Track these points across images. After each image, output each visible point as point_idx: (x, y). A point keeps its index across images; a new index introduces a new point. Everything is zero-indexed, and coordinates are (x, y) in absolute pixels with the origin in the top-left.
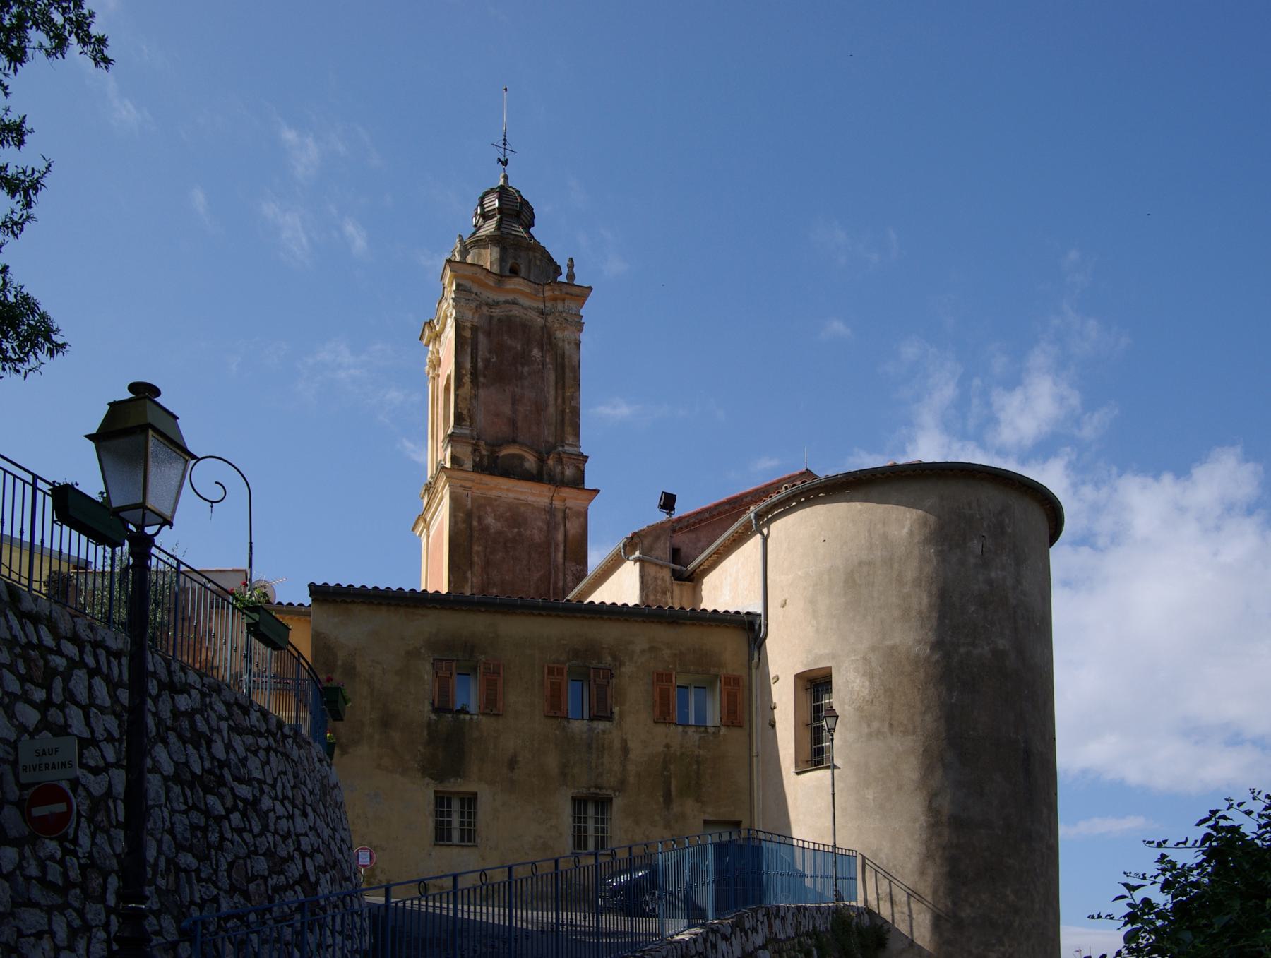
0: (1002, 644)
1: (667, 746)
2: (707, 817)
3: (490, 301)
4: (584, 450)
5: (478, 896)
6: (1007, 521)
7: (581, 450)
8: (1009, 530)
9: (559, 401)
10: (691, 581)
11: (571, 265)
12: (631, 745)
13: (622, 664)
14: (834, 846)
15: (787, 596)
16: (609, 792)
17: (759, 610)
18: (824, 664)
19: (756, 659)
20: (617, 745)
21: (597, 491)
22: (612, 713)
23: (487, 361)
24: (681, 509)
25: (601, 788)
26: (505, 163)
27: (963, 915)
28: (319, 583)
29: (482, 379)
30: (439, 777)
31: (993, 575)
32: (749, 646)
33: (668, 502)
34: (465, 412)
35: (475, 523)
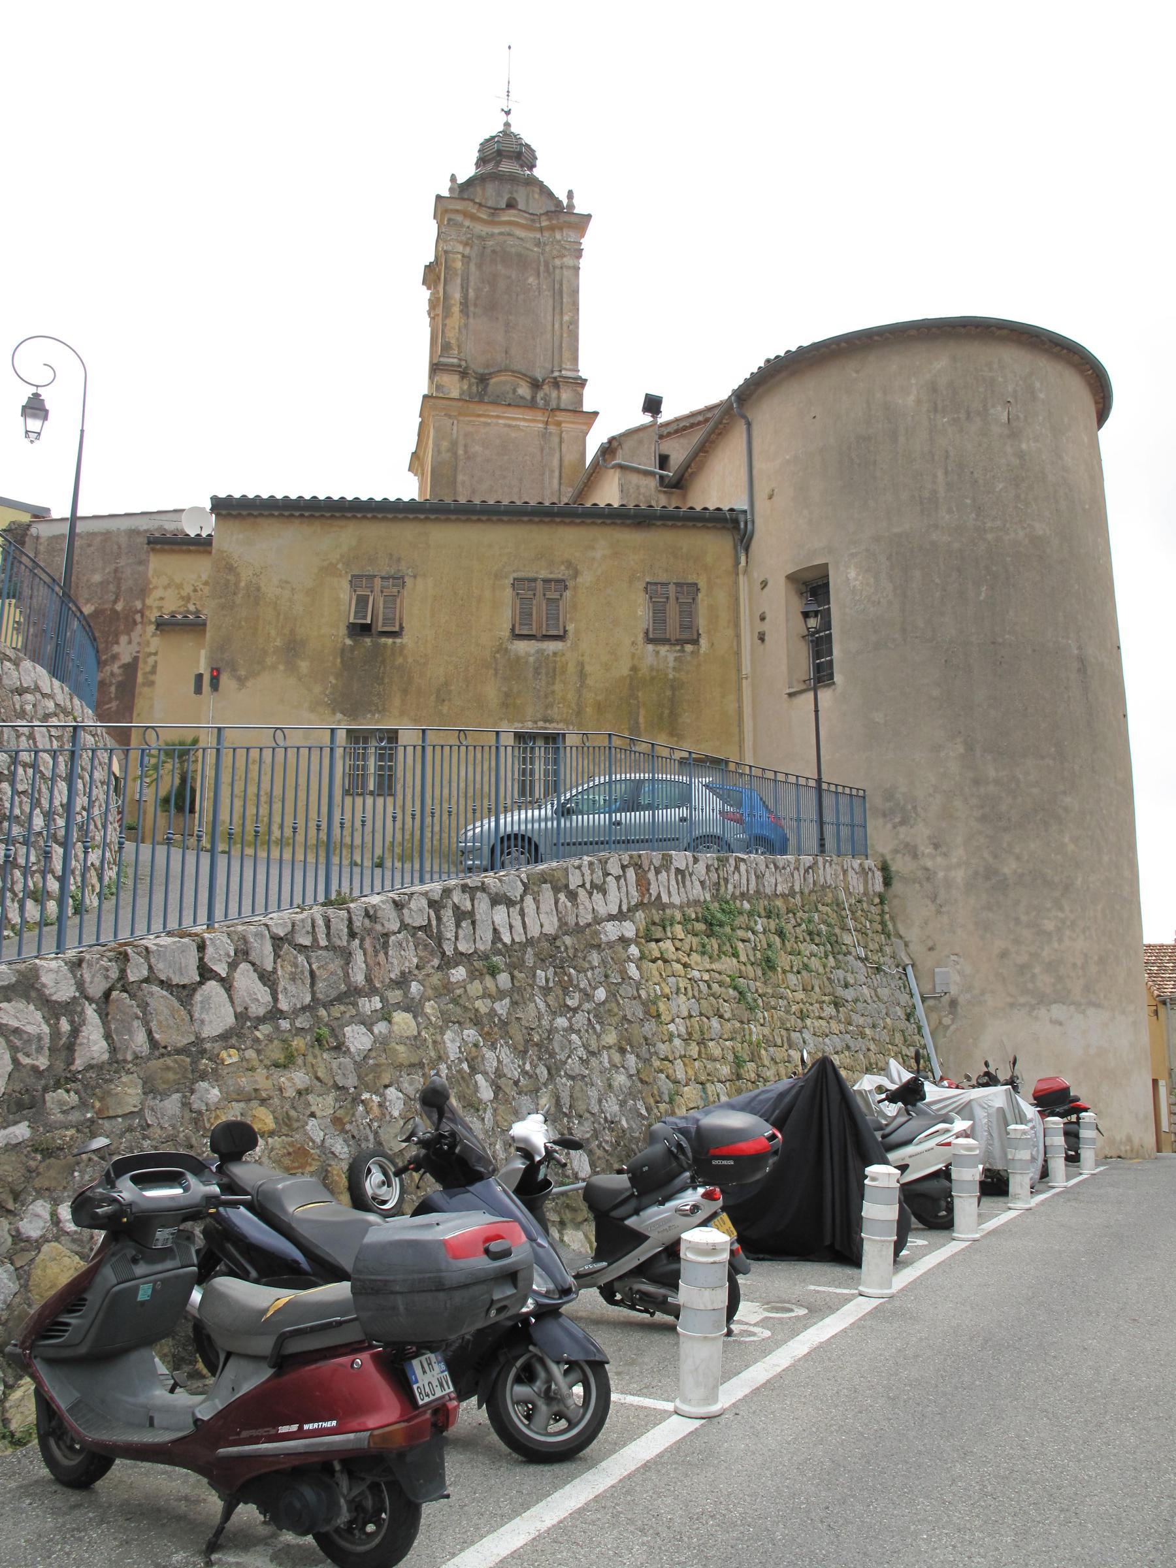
0: (1040, 528)
1: (634, 669)
3: (483, 233)
4: (583, 374)
6: (1038, 385)
8: (1042, 396)
12: (588, 668)
13: (576, 574)
14: (819, 781)
17: (742, 504)
19: (743, 562)
20: (572, 668)
21: (596, 414)
22: (565, 631)
23: (478, 290)
24: (668, 413)
25: (551, 721)
26: (508, 113)
27: (1006, 870)
28: (222, 495)
29: (472, 309)
30: (352, 712)
31: (1024, 446)
32: (735, 547)
33: (652, 405)
34: (453, 341)
35: (461, 452)
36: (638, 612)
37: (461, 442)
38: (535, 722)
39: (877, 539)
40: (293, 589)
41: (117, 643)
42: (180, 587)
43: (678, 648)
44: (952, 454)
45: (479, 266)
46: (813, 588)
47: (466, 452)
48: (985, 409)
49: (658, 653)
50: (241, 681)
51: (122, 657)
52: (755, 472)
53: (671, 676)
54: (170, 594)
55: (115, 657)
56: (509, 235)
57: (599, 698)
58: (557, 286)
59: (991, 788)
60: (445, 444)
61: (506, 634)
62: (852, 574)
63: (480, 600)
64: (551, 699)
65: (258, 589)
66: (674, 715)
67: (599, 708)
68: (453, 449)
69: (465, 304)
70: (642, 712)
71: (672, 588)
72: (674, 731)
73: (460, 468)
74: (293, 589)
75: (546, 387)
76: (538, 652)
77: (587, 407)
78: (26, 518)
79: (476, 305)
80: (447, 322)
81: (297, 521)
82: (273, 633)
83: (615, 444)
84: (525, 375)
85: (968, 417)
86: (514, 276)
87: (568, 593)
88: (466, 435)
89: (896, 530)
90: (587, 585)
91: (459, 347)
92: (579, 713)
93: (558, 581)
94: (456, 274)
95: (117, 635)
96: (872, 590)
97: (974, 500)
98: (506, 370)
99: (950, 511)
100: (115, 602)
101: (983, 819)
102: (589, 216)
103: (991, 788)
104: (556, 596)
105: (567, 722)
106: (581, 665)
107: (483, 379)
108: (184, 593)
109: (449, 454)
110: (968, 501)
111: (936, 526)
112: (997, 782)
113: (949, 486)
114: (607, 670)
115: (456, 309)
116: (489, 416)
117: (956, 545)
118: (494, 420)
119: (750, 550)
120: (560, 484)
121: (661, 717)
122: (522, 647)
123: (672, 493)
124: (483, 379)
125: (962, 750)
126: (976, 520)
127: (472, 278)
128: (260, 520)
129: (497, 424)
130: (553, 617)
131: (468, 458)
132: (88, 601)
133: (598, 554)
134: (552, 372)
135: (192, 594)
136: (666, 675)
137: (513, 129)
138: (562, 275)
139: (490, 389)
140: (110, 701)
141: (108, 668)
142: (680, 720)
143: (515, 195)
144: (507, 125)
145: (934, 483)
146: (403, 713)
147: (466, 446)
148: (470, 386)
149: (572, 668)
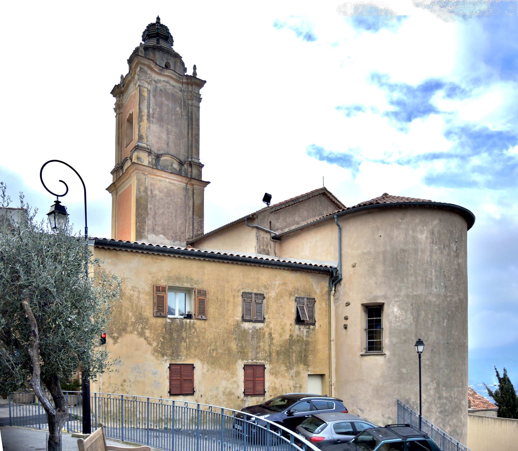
1: (291, 336)
2: (309, 373)
3: (156, 79)
4: (202, 161)
5: (183, 421)
7: (200, 161)
9: (190, 135)
10: (279, 240)
11: (195, 67)
15: (356, 261)
16: (263, 361)
18: (380, 301)
20: (267, 335)
21: (209, 183)
22: (264, 318)
24: (273, 202)
29: (151, 119)
32: (329, 283)
33: (267, 198)
34: (144, 135)
35: (149, 193)
36: (291, 309)
37: (149, 188)
38: (252, 360)
39: (408, 296)
40: (139, 292)
43: (308, 327)
44: (438, 263)
45: (154, 96)
46: (374, 312)
47: (152, 193)
48: (450, 245)
49: (300, 329)
50: (115, 340)
52: (343, 252)
56: (167, 82)
57: (277, 349)
58: (190, 115)
59: (444, 401)
60: (142, 189)
61: (239, 319)
62: (396, 309)
63: (228, 302)
64: (258, 350)
66: (306, 356)
67: (278, 353)
69: (148, 116)
70: (294, 355)
71: (305, 299)
72: (306, 363)
73: (149, 201)
74: (139, 292)
75: (185, 165)
76: (253, 328)
77: (204, 179)
79: (153, 117)
80: (141, 124)
81: (139, 255)
82: (130, 314)
83: (255, 216)
84: (177, 158)
85: (444, 247)
86: (170, 105)
87: (265, 301)
88: (151, 185)
89: (415, 293)
90: (273, 297)
92: (270, 356)
93: (261, 295)
96: (404, 318)
97: (444, 283)
98: (169, 154)
99: (436, 288)
101: (441, 412)
102: (205, 82)
103: (444, 401)
104: (260, 301)
105: (264, 359)
106: (270, 334)
107: (158, 157)
110: (442, 284)
111: (431, 294)
112: (446, 398)
113: (436, 276)
114: (281, 336)
115: (145, 118)
116: (162, 177)
117: (437, 303)
118: (164, 179)
120: (193, 214)
121: (301, 357)
122: (247, 325)
123: (276, 242)
124: (158, 157)
125: (435, 386)
126: (444, 292)
127: (151, 102)
128: (120, 253)
129: (165, 181)
130: (260, 311)
133: (277, 283)
134: (188, 158)
136: (303, 339)
137: (162, 22)
138: (192, 109)
139: (161, 162)
142: (308, 359)
143: (169, 61)
145: (431, 275)
146: (195, 356)
147: (151, 190)
148: (152, 159)
149: (267, 335)
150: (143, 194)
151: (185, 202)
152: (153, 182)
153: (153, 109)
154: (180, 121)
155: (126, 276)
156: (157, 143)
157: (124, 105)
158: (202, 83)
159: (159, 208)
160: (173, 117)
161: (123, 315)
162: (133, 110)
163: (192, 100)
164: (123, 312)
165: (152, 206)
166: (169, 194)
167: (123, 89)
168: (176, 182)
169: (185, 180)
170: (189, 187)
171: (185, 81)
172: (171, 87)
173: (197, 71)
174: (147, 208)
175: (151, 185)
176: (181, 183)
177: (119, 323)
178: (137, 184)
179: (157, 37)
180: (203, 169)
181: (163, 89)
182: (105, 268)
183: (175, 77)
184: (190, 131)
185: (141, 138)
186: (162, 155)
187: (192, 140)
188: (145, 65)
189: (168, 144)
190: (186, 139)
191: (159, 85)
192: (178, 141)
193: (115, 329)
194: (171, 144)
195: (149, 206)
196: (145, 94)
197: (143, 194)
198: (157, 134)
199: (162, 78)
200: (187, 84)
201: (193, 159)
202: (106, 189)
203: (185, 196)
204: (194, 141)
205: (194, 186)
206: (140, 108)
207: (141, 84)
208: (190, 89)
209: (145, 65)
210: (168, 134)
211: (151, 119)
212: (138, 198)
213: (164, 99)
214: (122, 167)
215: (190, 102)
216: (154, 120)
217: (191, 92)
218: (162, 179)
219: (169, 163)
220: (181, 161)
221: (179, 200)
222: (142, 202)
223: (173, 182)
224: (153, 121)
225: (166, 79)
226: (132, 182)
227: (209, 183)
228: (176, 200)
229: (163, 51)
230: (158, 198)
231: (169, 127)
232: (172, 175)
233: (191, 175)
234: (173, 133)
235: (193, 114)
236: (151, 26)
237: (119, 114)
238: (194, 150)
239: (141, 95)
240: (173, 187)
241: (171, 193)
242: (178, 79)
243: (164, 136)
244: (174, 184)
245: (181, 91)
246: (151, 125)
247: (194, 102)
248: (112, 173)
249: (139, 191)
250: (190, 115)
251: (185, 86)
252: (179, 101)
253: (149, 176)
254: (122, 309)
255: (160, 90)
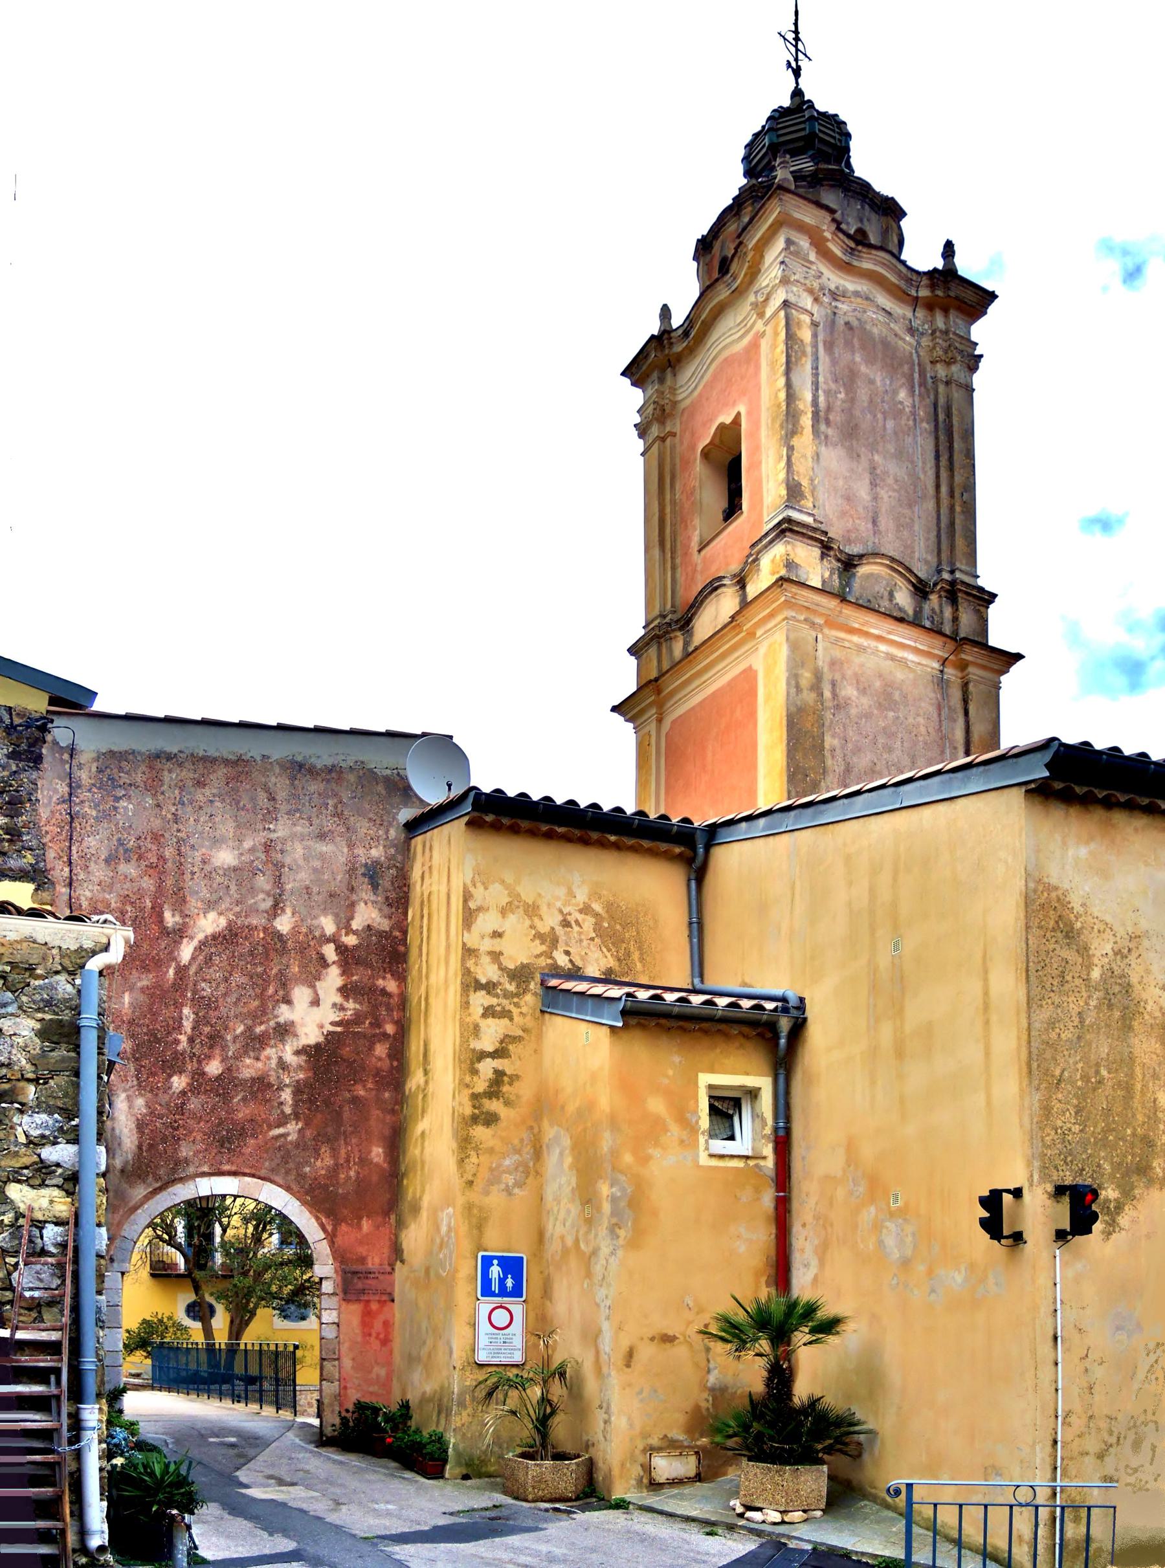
7: (980, 582)
9: (944, 489)
21: (1019, 657)
29: (823, 427)
34: (805, 483)
35: (827, 694)
37: (827, 676)
41: (288, 1001)
42: (532, 911)
45: (829, 346)
47: (835, 695)
51: (301, 1031)
53: (180, 1048)
54: (514, 924)
55: (285, 1031)
58: (941, 417)
60: (806, 676)
65: (1127, 988)
68: (816, 687)
69: (816, 415)
73: (827, 724)
75: (934, 597)
78: (36, 703)
79: (828, 422)
80: (795, 442)
86: (878, 380)
88: (833, 663)
91: (813, 492)
94: (804, 353)
95: (284, 984)
98: (876, 554)
100: (276, 909)
108: (543, 928)
109: (813, 695)
115: (806, 421)
116: (867, 635)
118: (873, 644)
119: (710, 878)
124: (848, 564)
128: (1119, 817)
131: (838, 707)
132: (210, 905)
135: (560, 931)
139: (857, 584)
140: (282, 1121)
141: (269, 1051)
144: (797, 93)
147: (833, 684)
150: (809, 697)
151: (940, 729)
152: (837, 653)
153: (828, 393)
154: (909, 440)
155: (1144, 925)
156: (843, 514)
157: (683, 405)
158: (978, 301)
159: (858, 750)
160: (890, 424)
161: (1136, 1103)
162: (742, 409)
163: (949, 363)
164: (1138, 1086)
165: (836, 742)
166: (888, 698)
167: (678, 348)
168: (911, 657)
169: (937, 646)
170: (951, 673)
171: (924, 293)
172: (881, 317)
173: (957, 260)
174: (822, 748)
175: (833, 663)
176: (925, 661)
177: (1123, 1139)
178: (789, 657)
179: (801, 152)
180: (993, 611)
181: (855, 323)
182: (1066, 886)
183: (893, 278)
184: (944, 474)
185: (794, 492)
186: (861, 556)
187: (952, 508)
188: (801, 227)
189: (874, 522)
190: (930, 505)
191: (843, 307)
192: (907, 512)
193: (1107, 1166)
194: (885, 522)
195: (829, 742)
196: (806, 335)
197: (809, 697)
198: (841, 483)
199: (850, 284)
200: (930, 306)
201: (958, 575)
202: (614, 709)
203: (939, 708)
204: (958, 509)
205: (971, 669)
206: (789, 385)
207: (792, 299)
208: (940, 322)
209: (801, 227)
210: (873, 485)
211: (823, 427)
212: (793, 709)
213: (858, 359)
214: (685, 623)
215: (941, 371)
216: (830, 432)
217: (946, 332)
218: (864, 642)
219: (881, 588)
220: (920, 580)
221: (921, 720)
222: (808, 724)
223: (900, 653)
224: (826, 437)
225: (862, 286)
226: (758, 661)
227: (1019, 657)
228: (911, 720)
229: (846, 190)
230: (853, 711)
231: (876, 457)
232: (902, 629)
233: (956, 632)
234: (890, 481)
235: (955, 412)
236: (779, 115)
237: (663, 439)
238: (960, 542)
239: (790, 337)
240: (900, 675)
241: (897, 696)
242: (902, 284)
243: (863, 492)
244: (903, 662)
245: (911, 330)
246: (823, 449)
247: (954, 368)
248: (635, 650)
249: (798, 686)
250: (941, 417)
251: (921, 313)
252: (906, 368)
253: (826, 631)
254: (1131, 1075)
255: (847, 323)
